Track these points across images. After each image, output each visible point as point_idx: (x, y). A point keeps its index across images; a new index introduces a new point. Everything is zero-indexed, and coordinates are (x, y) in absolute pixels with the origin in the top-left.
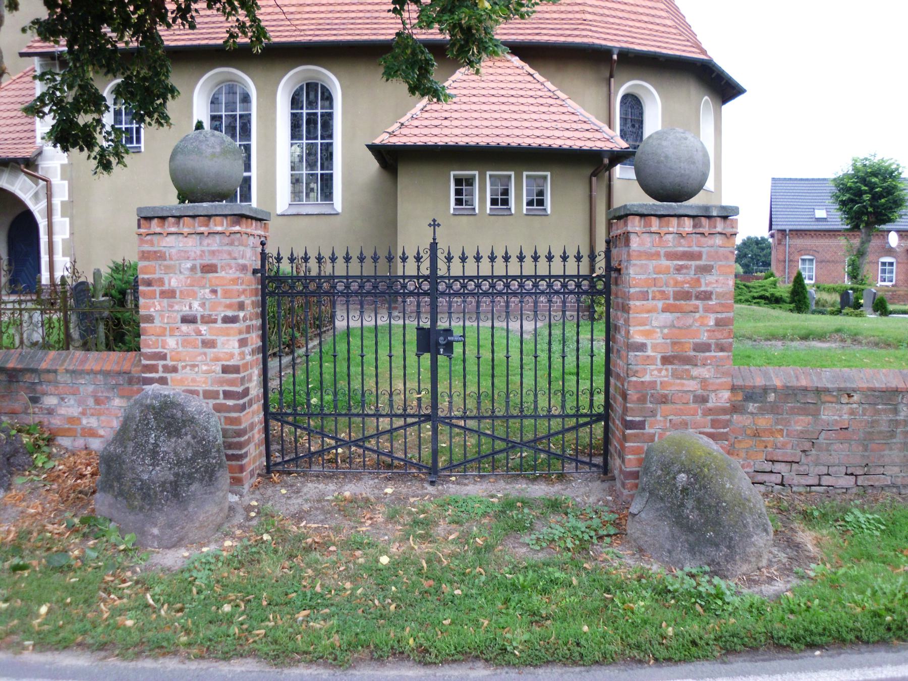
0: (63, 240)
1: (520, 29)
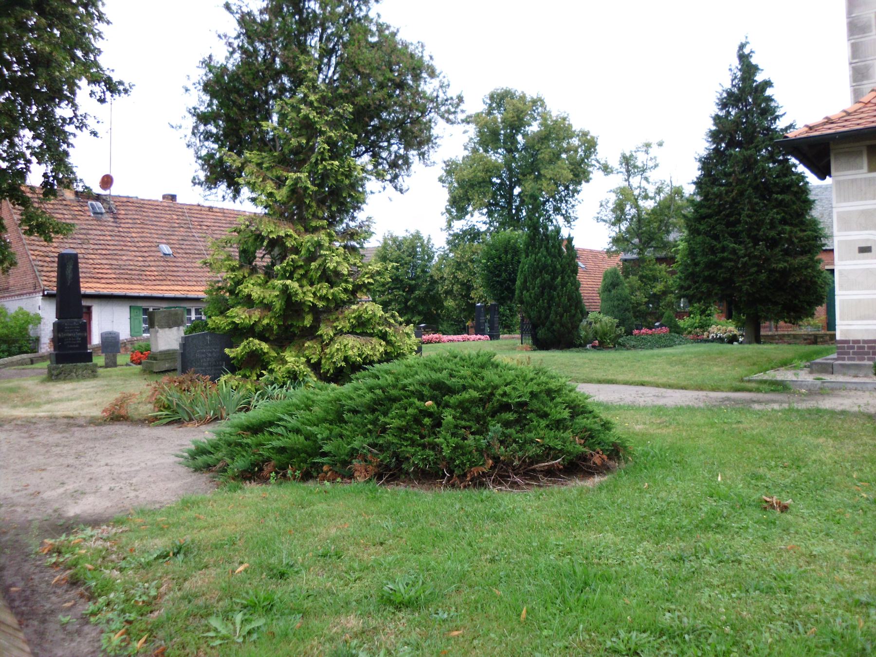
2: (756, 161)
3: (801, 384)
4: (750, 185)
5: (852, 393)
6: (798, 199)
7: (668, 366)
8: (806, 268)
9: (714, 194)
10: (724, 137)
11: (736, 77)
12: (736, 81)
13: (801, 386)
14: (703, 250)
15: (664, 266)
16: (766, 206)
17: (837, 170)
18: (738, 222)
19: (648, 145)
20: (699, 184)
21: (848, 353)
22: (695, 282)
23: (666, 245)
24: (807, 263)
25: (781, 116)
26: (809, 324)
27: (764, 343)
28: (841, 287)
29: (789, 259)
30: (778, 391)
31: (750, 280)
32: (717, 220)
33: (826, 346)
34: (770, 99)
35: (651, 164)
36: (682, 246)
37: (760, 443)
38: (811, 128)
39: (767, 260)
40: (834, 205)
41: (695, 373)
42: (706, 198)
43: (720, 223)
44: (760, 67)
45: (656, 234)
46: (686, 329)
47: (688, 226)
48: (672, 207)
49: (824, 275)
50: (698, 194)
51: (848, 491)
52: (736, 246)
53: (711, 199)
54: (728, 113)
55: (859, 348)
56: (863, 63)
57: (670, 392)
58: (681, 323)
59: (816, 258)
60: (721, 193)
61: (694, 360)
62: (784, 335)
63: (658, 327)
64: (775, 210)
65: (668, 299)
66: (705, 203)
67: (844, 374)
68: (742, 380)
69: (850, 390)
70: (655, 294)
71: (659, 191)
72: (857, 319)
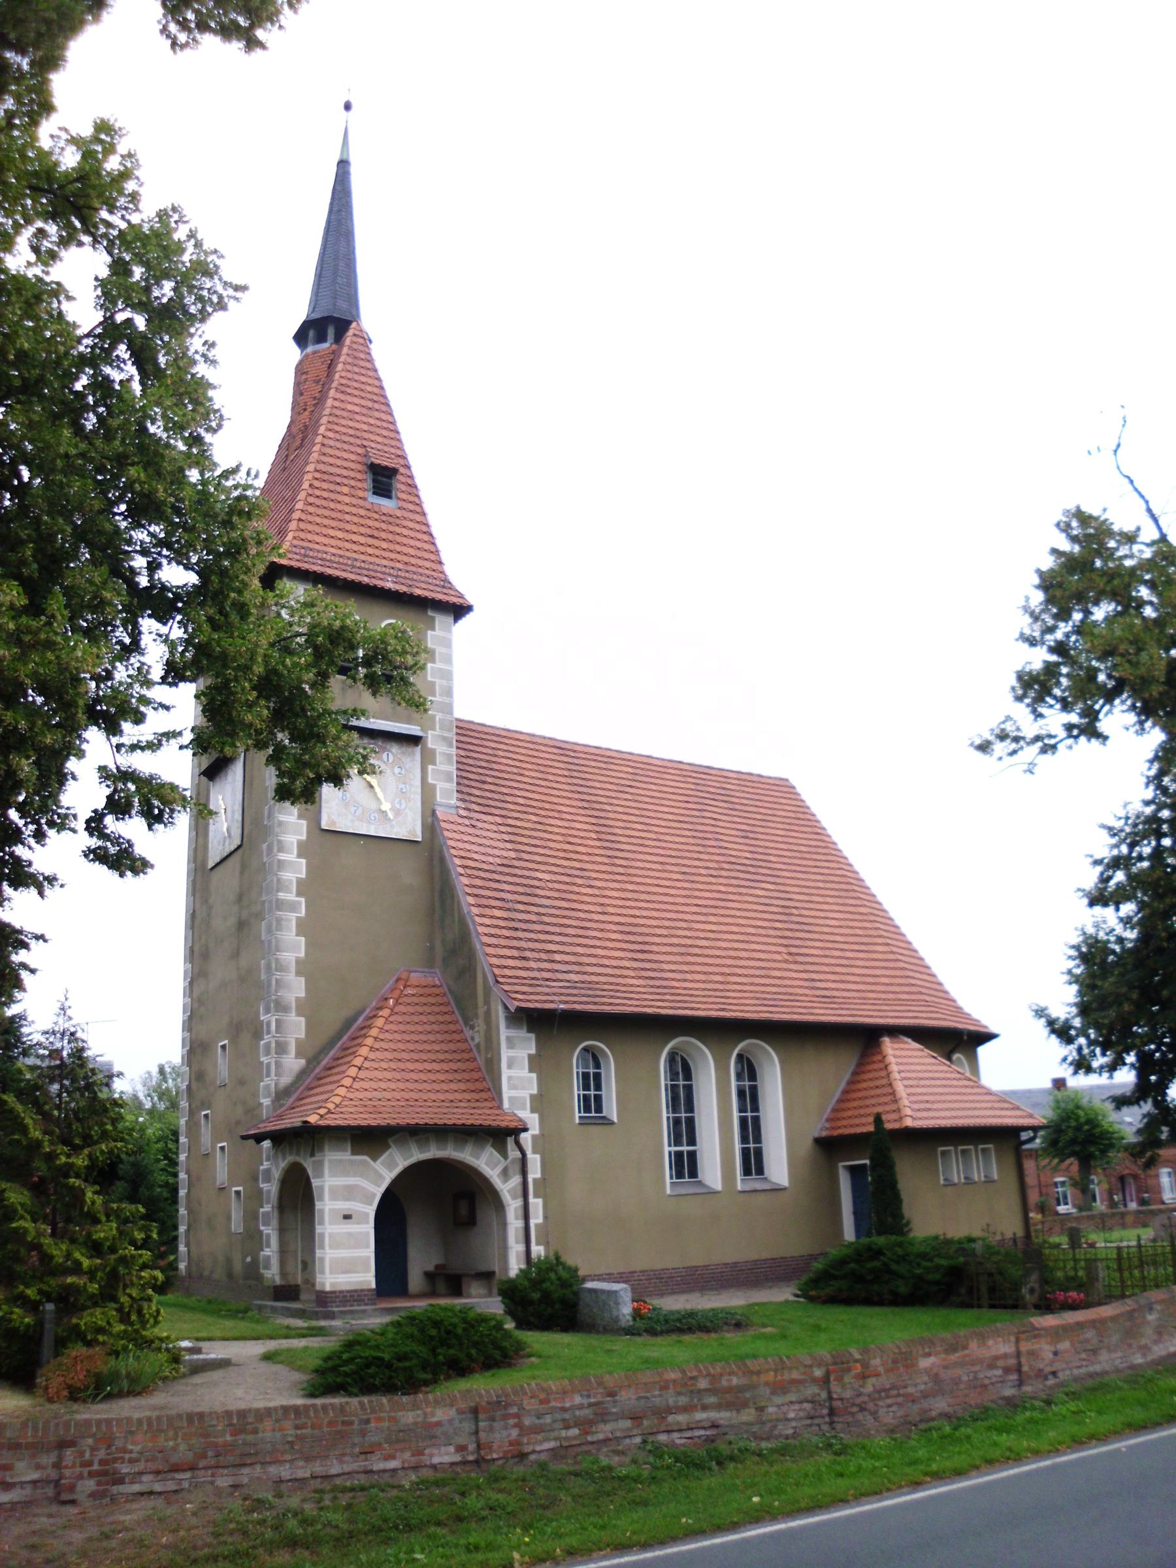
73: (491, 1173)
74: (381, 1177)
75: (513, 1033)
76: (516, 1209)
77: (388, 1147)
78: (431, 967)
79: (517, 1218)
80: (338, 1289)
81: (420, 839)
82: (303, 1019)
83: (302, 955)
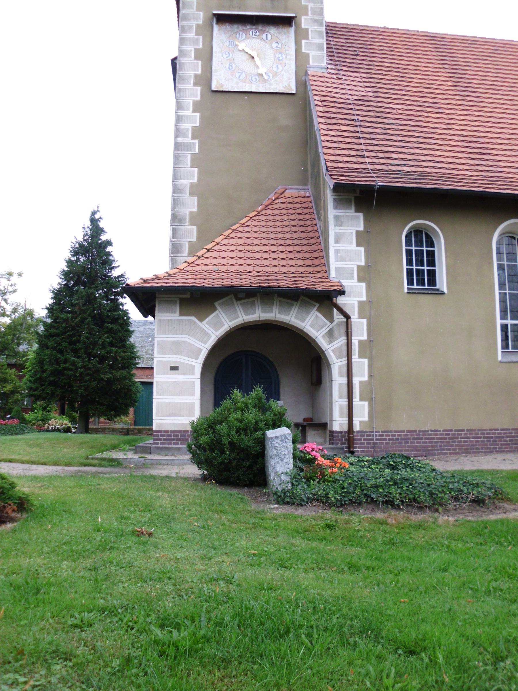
0: (361, 382)
1: (340, 113)
2: (96, 298)
3: (130, 461)
4: (89, 315)
5: (165, 467)
6: (123, 329)
7: (28, 448)
8: (125, 380)
9: (62, 318)
10: (74, 277)
11: (87, 234)
12: (87, 237)
13: (130, 463)
14: (50, 361)
15: (13, 371)
16: (99, 332)
17: (159, 312)
18: (79, 341)
19: (10, 274)
20: (51, 310)
21: (161, 440)
22: (42, 385)
23: (16, 354)
24: (126, 376)
25: (116, 267)
26: (121, 421)
27: (91, 433)
28: (158, 393)
29: (114, 371)
30: (114, 466)
31: (84, 385)
32: (63, 338)
33: (135, 437)
34: (109, 254)
35: (11, 289)
36: (31, 356)
37: (119, 496)
38: (145, 281)
39: (97, 371)
40: (156, 335)
41: (50, 453)
42: (55, 321)
43: (64, 341)
44: (105, 230)
45: (9, 344)
46: (30, 421)
47: (39, 341)
48: (24, 325)
49: (136, 385)
50: (49, 317)
51: (186, 523)
52: (76, 359)
53: (59, 322)
54: (78, 259)
55: (168, 436)
56: (179, 242)
57: (34, 467)
58: (27, 416)
59: (132, 372)
60: (68, 318)
61: (47, 443)
62: (105, 429)
63: (9, 419)
64: (106, 335)
65: (15, 397)
66: (55, 325)
67: (158, 454)
68: (87, 458)
69: (164, 465)
70: (5, 393)
71: (15, 310)
72: (167, 416)
73: (317, 334)
74: (207, 335)
75: (341, 212)
76: (340, 367)
77: (215, 309)
78: (305, 184)
79: (341, 375)
80: (163, 429)
81: (294, 92)
82: (195, 228)
83: (196, 180)
